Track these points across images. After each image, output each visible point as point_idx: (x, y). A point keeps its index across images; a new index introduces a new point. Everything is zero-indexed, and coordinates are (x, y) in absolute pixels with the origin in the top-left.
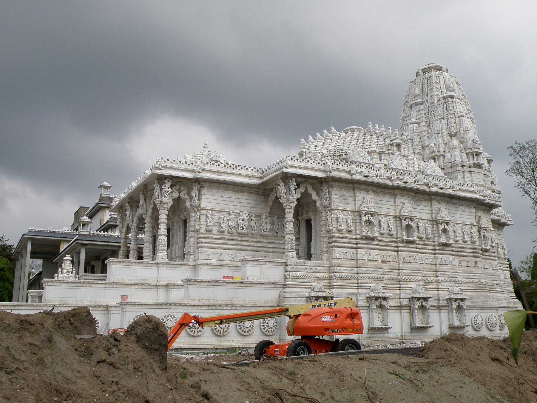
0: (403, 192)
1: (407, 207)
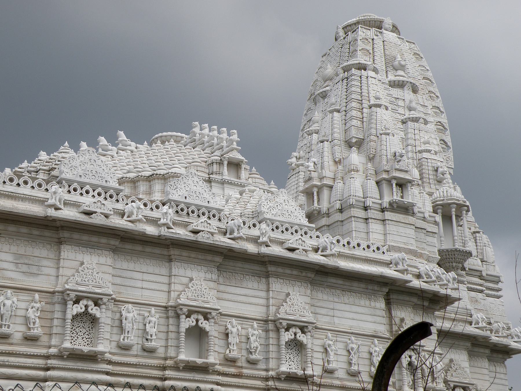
1: (196, 285)
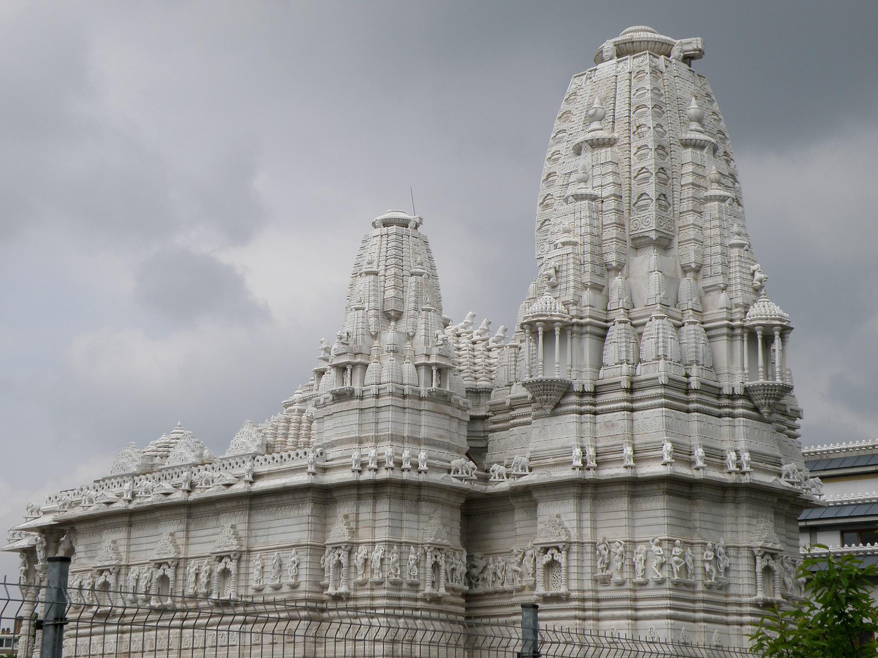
0: (168, 513)
